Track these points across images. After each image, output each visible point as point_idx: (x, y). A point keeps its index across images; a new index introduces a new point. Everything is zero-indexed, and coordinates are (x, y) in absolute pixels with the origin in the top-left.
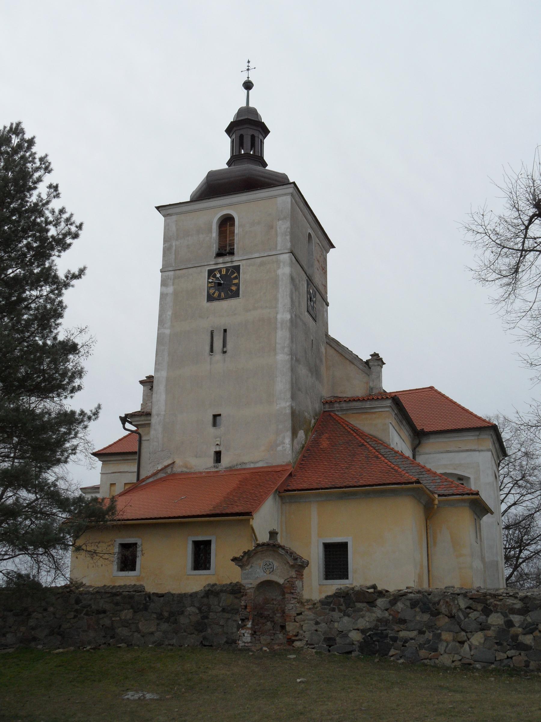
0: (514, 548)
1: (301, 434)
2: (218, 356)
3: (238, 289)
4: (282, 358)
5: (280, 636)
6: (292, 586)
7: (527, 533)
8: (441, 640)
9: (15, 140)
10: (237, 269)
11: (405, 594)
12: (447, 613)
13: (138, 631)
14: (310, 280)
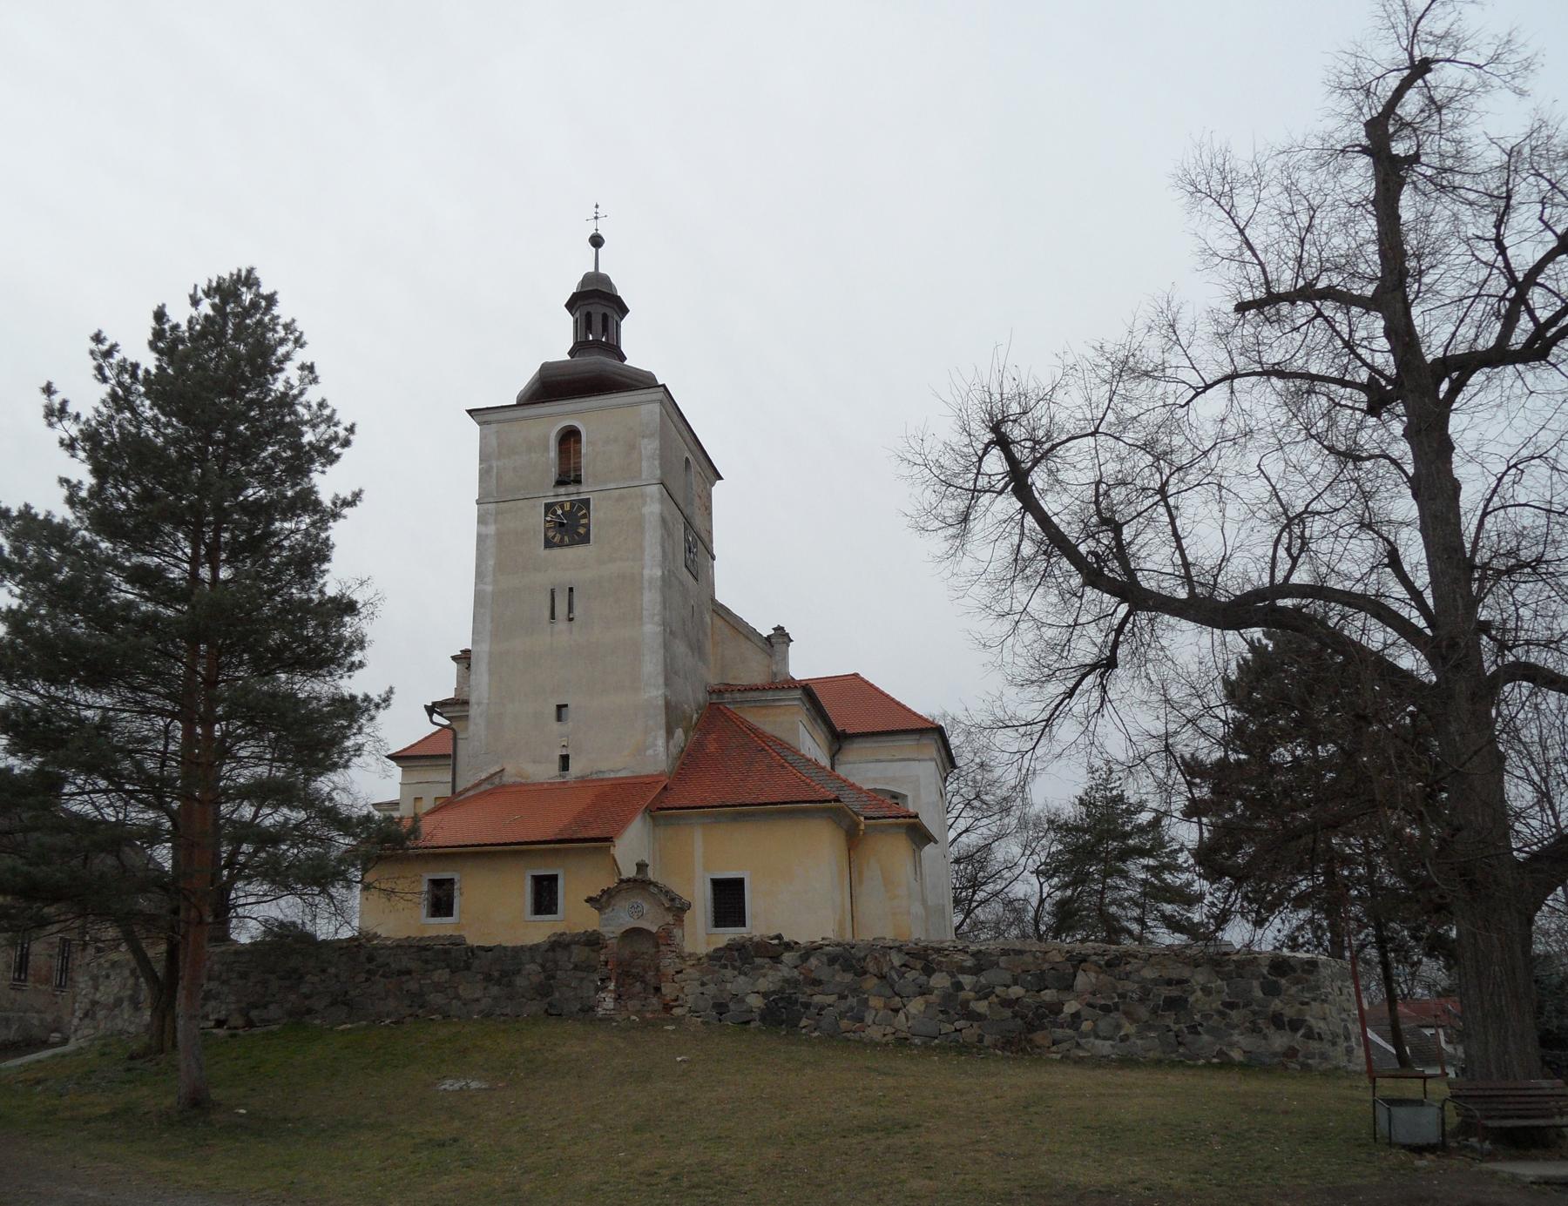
0: (966, 888)
1: (679, 733)
2: (562, 624)
4: (651, 629)
5: (654, 1000)
6: (669, 935)
7: (982, 868)
8: (868, 1007)
9: (247, 297)
11: (821, 947)
13: (458, 997)
14: (688, 523)
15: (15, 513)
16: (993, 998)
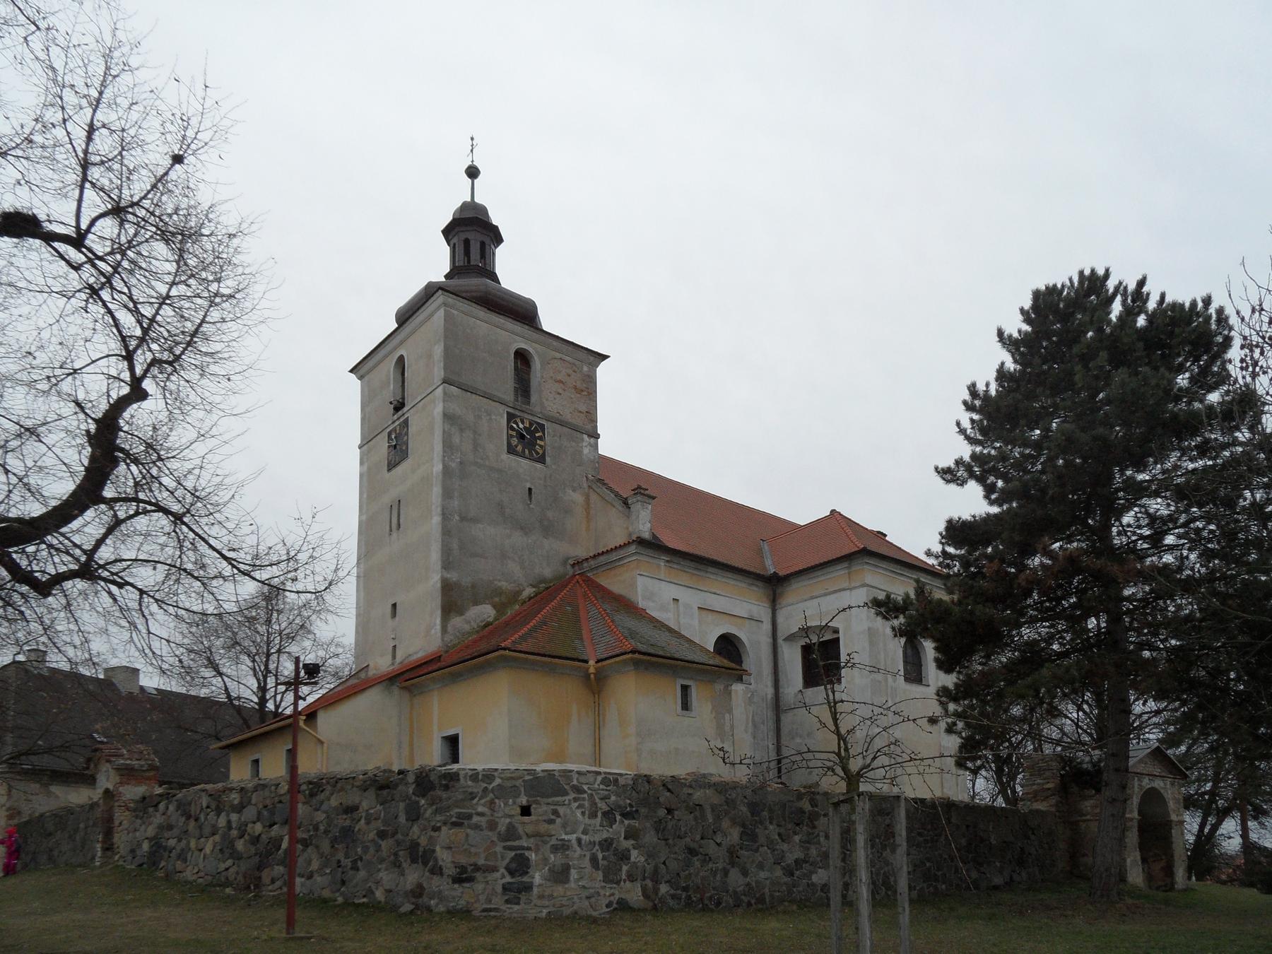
15: (953, 466)
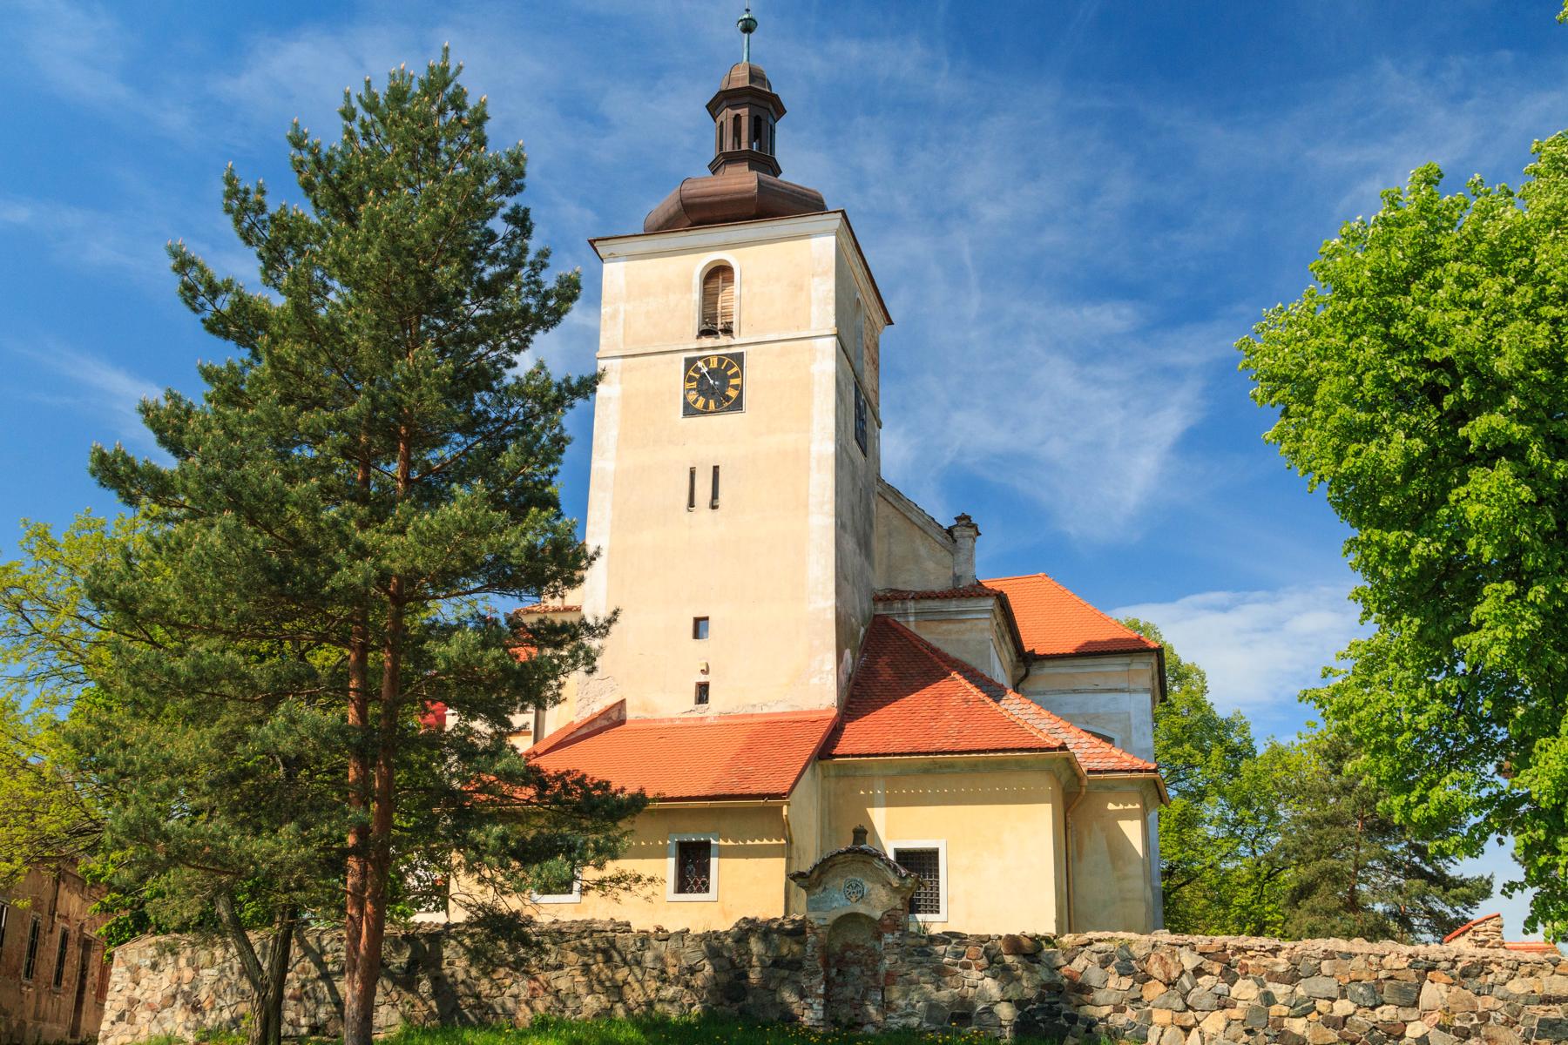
1: (847, 652)
3: (740, 397)
10: (739, 358)
12: (1162, 977)
16: (1313, 1016)
